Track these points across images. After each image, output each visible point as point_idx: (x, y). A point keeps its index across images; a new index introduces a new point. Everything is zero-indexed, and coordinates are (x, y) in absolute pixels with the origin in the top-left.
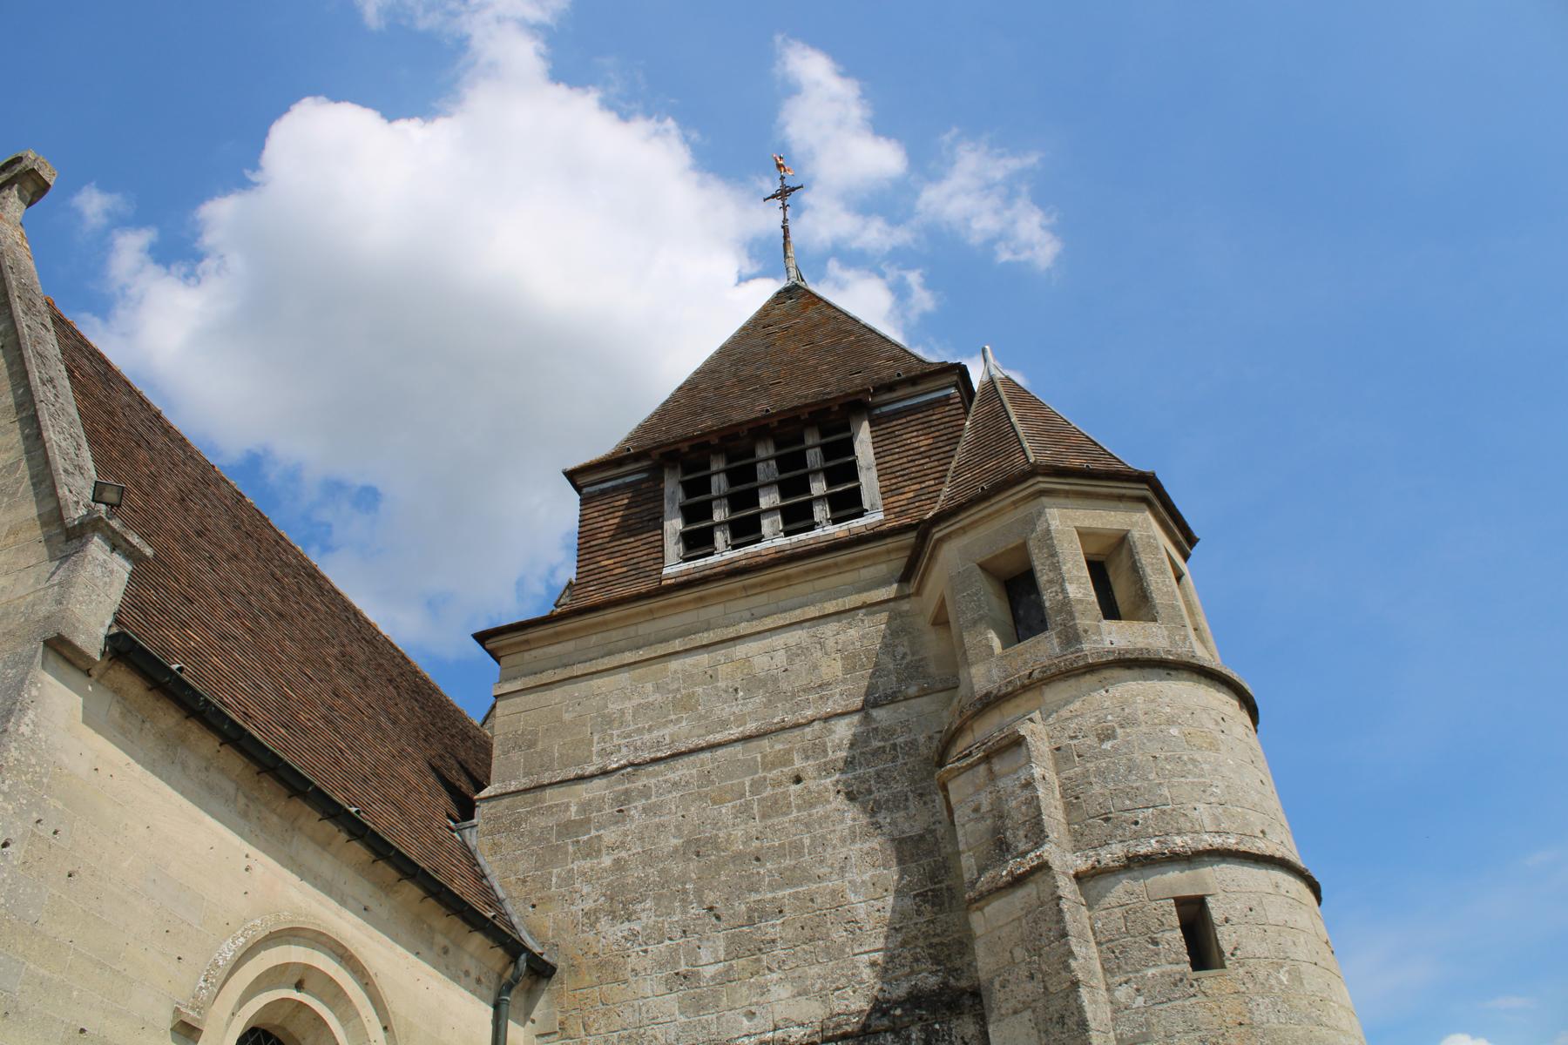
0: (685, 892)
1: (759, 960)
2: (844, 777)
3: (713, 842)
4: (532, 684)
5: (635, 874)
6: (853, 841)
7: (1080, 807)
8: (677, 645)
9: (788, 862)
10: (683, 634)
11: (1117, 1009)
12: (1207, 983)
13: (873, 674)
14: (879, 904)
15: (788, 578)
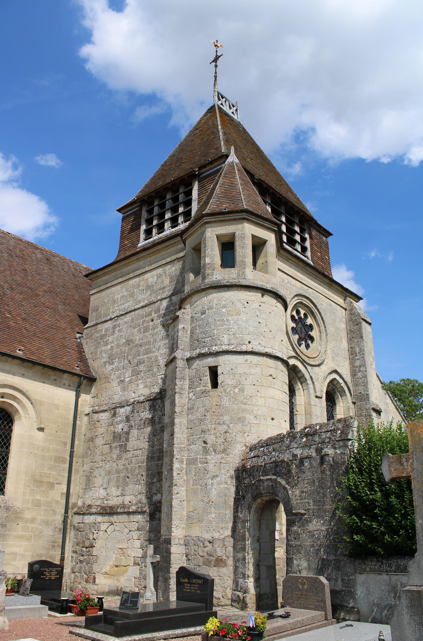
0: (124, 356)
1: (138, 377)
3: (132, 341)
4: (98, 290)
8: (131, 275)
9: (147, 347)
10: (133, 272)
13: (176, 283)
15: (159, 250)
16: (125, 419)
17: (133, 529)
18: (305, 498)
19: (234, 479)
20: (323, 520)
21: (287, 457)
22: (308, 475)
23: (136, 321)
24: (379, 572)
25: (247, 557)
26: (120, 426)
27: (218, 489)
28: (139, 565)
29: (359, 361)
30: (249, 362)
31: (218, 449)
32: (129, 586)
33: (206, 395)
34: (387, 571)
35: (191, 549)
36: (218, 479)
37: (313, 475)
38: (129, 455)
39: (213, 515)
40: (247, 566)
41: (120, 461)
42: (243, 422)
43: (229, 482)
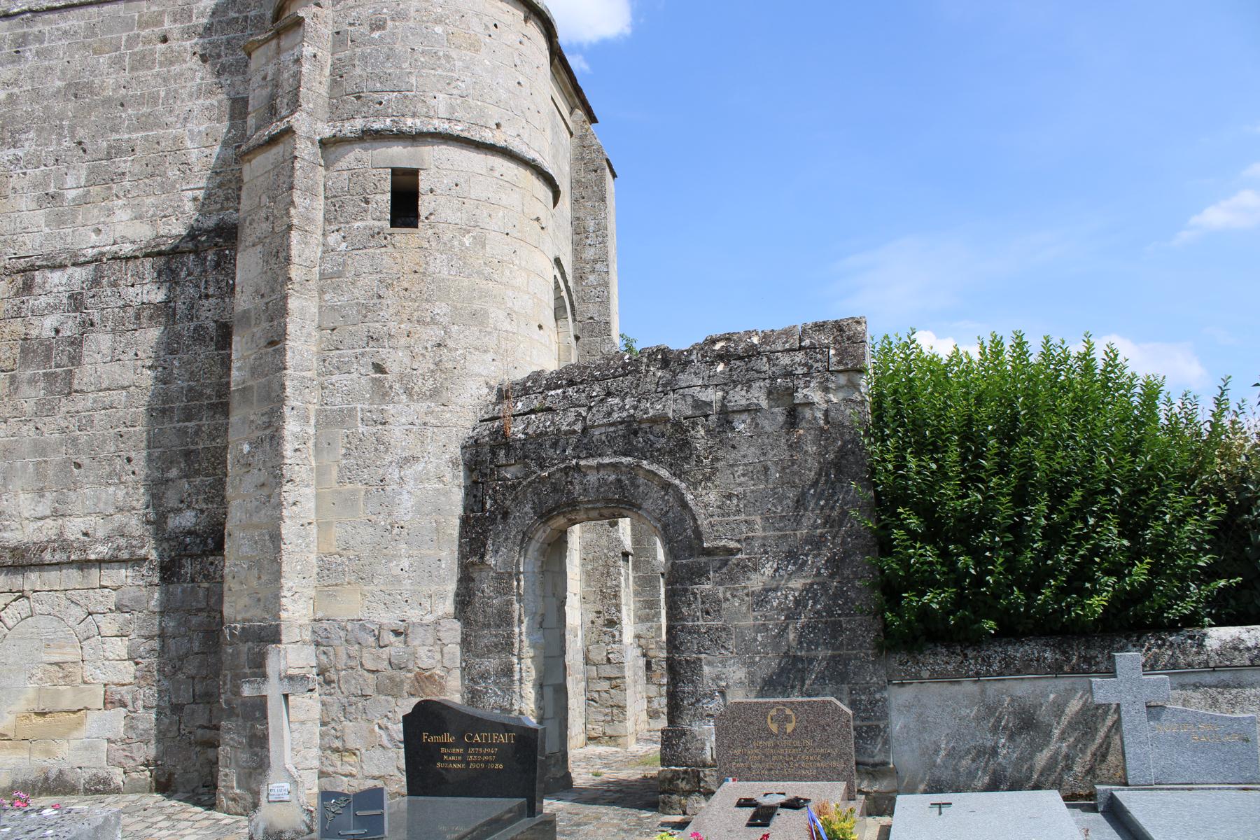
0: (61, 127)
1: (110, 188)
2: (201, 41)
3: (89, 87)
5: (24, 108)
6: (198, 97)
7: (341, 85)
9: (145, 110)
11: (327, 250)
12: (398, 238)
14: (208, 151)
16: (65, 301)
17: (100, 609)
18: (739, 512)
19: (461, 467)
20: (794, 564)
21: (672, 407)
22: (749, 452)
23: (104, 33)
24: (955, 678)
25: (517, 668)
26: (50, 322)
27: (419, 492)
28: (125, 706)
29: (593, 249)
30: (497, 174)
31: (416, 389)
32: (91, 764)
33: (385, 242)
34: (978, 674)
35: (335, 655)
36: (419, 467)
37: (764, 454)
38: (83, 403)
39: (405, 563)
40: (516, 687)
41: (47, 420)
42: (481, 323)
43: (448, 478)
